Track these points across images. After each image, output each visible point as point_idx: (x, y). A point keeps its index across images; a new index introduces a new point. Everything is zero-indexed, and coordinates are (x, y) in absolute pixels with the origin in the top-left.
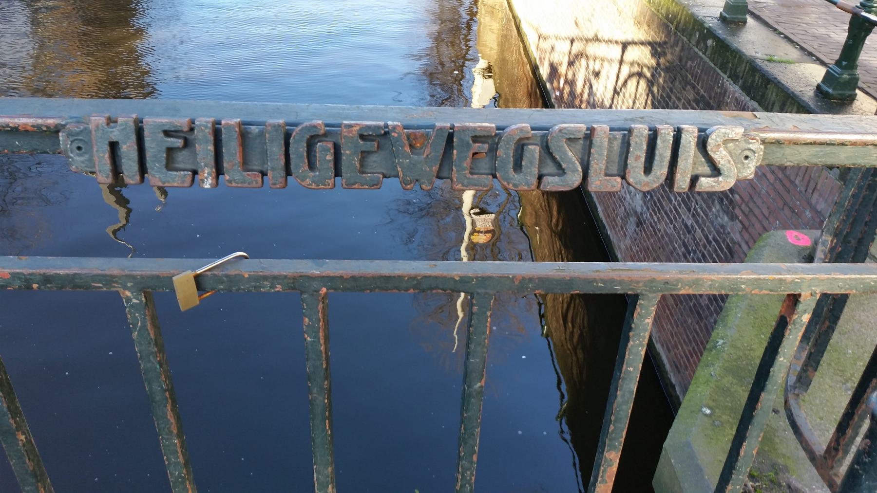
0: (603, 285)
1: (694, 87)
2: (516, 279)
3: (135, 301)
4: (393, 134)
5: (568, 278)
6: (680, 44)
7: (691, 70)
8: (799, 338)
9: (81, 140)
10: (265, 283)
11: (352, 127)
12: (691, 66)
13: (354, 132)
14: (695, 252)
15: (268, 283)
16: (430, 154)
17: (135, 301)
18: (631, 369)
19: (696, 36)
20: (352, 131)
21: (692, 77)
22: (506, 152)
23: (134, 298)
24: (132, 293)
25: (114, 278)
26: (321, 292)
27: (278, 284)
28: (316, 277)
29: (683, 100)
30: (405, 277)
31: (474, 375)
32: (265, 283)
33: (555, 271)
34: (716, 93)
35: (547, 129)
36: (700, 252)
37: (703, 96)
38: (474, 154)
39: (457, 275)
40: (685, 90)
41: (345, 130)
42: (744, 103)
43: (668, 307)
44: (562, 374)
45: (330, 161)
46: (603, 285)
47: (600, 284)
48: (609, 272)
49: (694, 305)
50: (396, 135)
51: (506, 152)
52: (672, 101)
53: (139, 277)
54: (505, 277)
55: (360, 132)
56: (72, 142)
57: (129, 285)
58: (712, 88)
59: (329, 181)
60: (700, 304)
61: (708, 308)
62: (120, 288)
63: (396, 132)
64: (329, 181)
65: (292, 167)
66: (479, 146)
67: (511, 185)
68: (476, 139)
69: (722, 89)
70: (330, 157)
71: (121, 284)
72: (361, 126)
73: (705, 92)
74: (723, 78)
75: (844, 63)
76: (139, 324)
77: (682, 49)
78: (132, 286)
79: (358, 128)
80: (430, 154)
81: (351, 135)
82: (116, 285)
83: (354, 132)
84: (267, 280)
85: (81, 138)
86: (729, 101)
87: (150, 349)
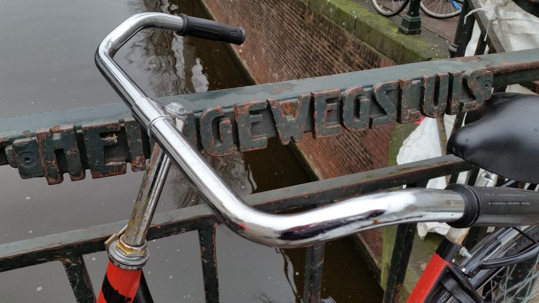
0: (396, 182)
1: (326, 38)
2: (344, 189)
3: (74, 265)
4: (273, 107)
5: (375, 182)
6: (313, 13)
7: (322, 28)
8: (517, 189)
9: (27, 152)
10: (173, 229)
11: (244, 106)
12: (322, 26)
13: (245, 110)
14: (343, 135)
15: (175, 229)
16: (299, 117)
17: (74, 265)
18: (411, 230)
19: (322, 7)
20: (244, 109)
21: (324, 32)
22: (348, 107)
23: (73, 263)
24: (71, 259)
25: (56, 251)
26: (214, 227)
27: (183, 228)
28: (210, 217)
29: (320, 47)
30: (272, 203)
31: (317, 257)
32: (173, 229)
33: (366, 178)
34: (340, 40)
35: (372, 86)
36: (346, 134)
37: (332, 43)
38: (328, 111)
39: (306, 195)
40: (320, 40)
41: (239, 110)
42: (358, 44)
43: (332, 169)
44: (513, 272)
45: (229, 134)
46: (396, 182)
47: (394, 182)
48: (399, 172)
49: (348, 166)
50: (275, 107)
51: (348, 107)
52: (314, 48)
53: (75, 246)
54: (337, 189)
55: (250, 110)
56: (20, 155)
57: (68, 254)
58: (337, 38)
59: (231, 149)
60: (351, 165)
61: (356, 166)
62: (61, 257)
63: (275, 105)
64: (231, 149)
65: (203, 143)
66: (332, 106)
67: (353, 129)
68: (329, 101)
69: (343, 37)
70: (230, 132)
71: (61, 254)
72: (250, 105)
73: (333, 40)
74: (343, 31)
75: (412, 13)
76: (78, 281)
77: (315, 16)
78: (70, 254)
79: (248, 107)
80: (299, 117)
81: (243, 112)
82: (58, 256)
83: (245, 110)
84: (174, 227)
85: (26, 151)
86: (349, 44)
87: (88, 296)
